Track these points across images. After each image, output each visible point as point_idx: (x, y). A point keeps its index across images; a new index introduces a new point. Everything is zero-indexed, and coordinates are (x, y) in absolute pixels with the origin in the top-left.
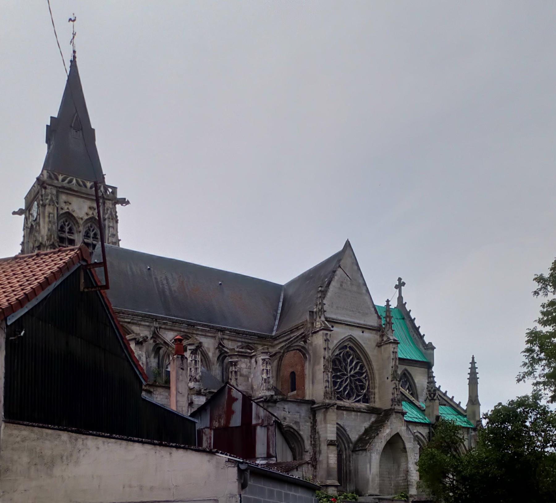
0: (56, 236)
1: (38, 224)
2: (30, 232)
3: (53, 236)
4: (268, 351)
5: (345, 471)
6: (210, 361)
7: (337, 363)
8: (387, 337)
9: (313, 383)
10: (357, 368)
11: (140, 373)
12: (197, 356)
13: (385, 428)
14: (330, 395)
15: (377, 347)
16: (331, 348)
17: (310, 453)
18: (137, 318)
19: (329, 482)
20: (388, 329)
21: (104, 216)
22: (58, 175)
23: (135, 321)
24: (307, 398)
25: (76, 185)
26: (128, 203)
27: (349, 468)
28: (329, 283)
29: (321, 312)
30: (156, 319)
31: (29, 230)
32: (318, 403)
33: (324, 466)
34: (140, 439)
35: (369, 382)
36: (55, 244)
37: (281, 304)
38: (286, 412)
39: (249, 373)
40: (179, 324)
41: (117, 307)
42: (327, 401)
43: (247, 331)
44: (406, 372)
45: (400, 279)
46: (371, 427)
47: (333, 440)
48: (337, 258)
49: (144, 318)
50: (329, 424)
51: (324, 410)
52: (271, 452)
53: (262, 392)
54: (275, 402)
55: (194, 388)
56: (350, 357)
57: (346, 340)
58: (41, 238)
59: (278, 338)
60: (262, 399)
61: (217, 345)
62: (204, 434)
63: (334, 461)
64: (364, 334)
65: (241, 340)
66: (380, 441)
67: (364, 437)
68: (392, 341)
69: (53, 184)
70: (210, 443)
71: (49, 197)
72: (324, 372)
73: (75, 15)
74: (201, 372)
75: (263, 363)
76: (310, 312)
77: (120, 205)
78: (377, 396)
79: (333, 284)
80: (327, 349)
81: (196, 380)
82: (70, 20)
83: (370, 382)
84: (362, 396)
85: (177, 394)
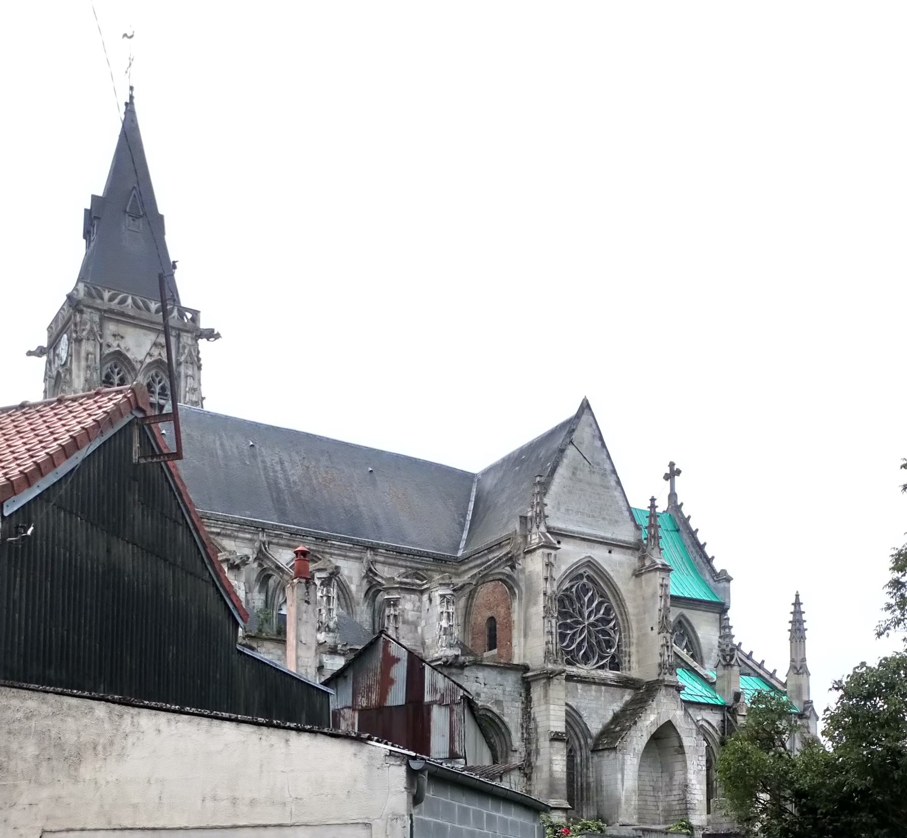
1: (69, 371)
2: (56, 383)
4: (450, 582)
5: (579, 784)
6: (353, 598)
7: (567, 602)
8: (651, 559)
9: (525, 636)
10: (600, 611)
12: (332, 589)
13: (649, 712)
15: (634, 577)
17: (520, 753)
18: (232, 526)
19: (552, 803)
23: (229, 532)
25: (132, 307)
26: (217, 336)
28: (554, 470)
29: (540, 519)
30: (262, 528)
31: (53, 381)
33: (545, 775)
34: (234, 716)
35: (620, 635)
37: (471, 506)
39: (418, 618)
40: (301, 537)
42: (550, 666)
44: (682, 620)
45: (672, 465)
46: (623, 710)
47: (559, 733)
48: (569, 427)
49: (242, 527)
51: (545, 681)
52: (457, 749)
53: (440, 651)
55: (325, 642)
56: (588, 593)
59: (466, 561)
60: (439, 662)
62: (341, 719)
65: (404, 563)
66: (640, 735)
68: (660, 566)
69: (95, 306)
71: (88, 327)
72: (544, 618)
75: (442, 602)
76: (521, 517)
81: (329, 630)
82: (125, 35)
83: (623, 634)
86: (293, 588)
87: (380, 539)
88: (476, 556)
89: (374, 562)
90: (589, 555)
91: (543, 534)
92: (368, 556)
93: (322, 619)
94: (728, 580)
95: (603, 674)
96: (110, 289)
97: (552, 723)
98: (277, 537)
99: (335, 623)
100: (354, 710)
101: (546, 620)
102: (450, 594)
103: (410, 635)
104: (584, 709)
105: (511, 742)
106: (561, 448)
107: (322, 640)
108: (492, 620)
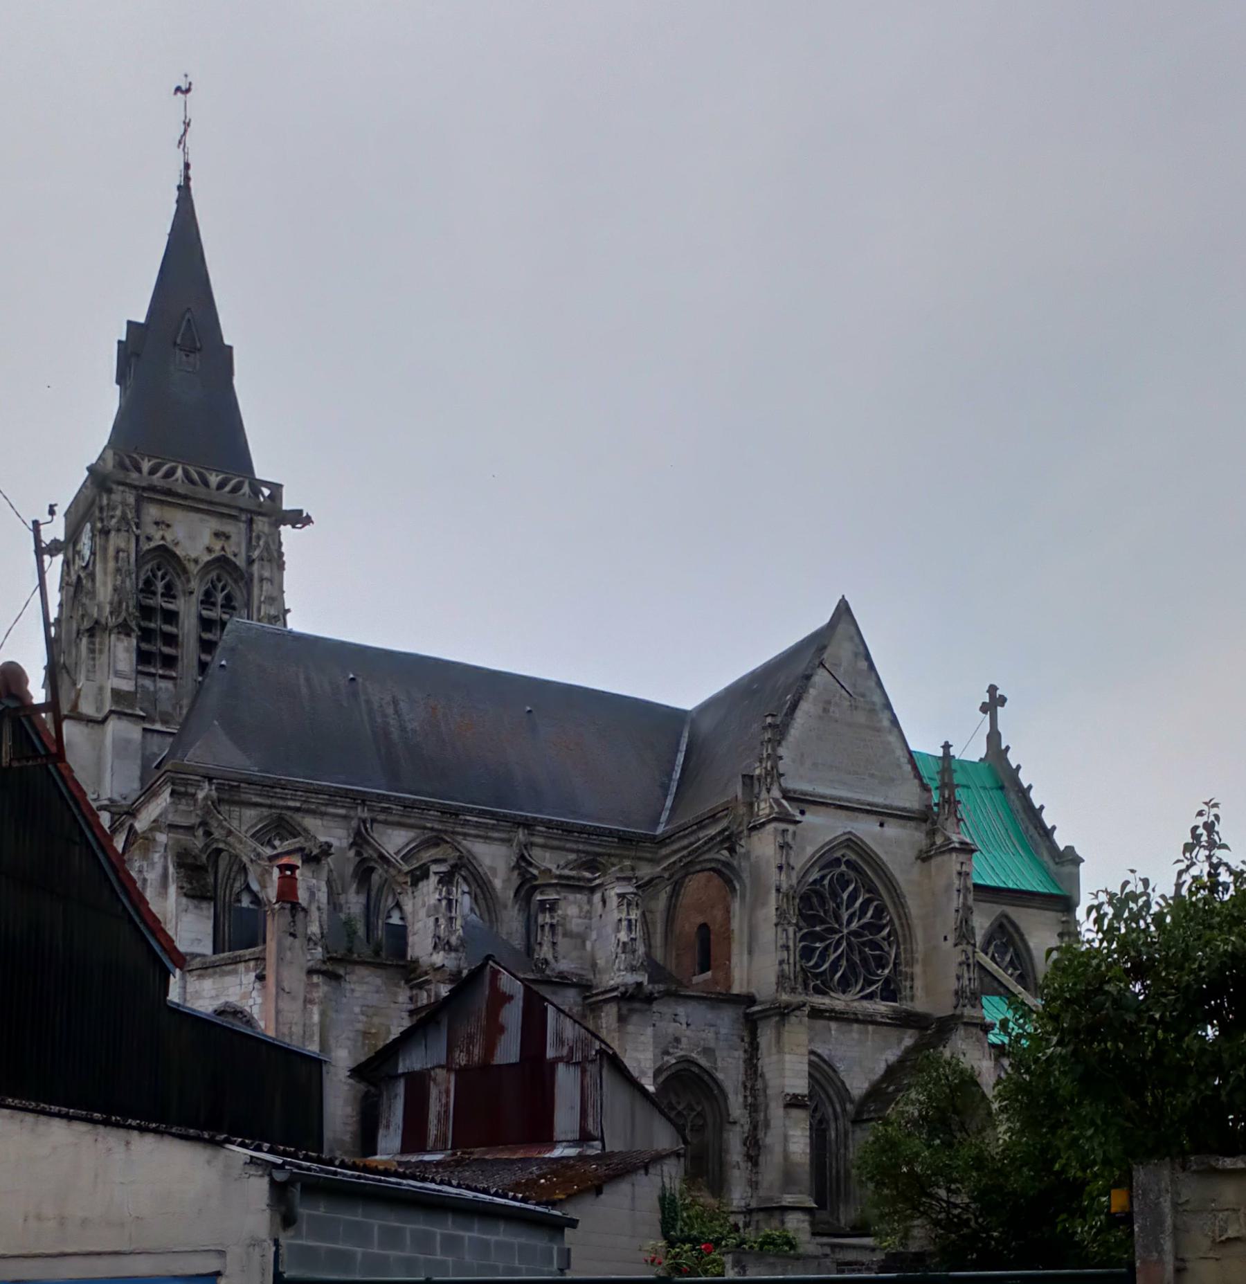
0: (132, 603)
1: (92, 576)
2: (75, 592)
3: (124, 604)
4: (632, 876)
5: (834, 1171)
6: (497, 897)
7: (815, 900)
8: (944, 835)
10: (866, 913)
11: (164, 949)
12: (454, 889)
14: (793, 983)
15: (919, 861)
16: (798, 866)
17: (742, 1126)
18: (317, 798)
19: (788, 1200)
20: (946, 816)
21: (251, 554)
22: (140, 460)
24: (736, 990)
25: (183, 481)
26: (308, 520)
27: (845, 1164)
28: (794, 706)
29: (772, 778)
30: (362, 799)
31: (72, 589)
32: (762, 1003)
33: (777, 1157)
34: (64, 1110)
35: (898, 948)
36: (129, 622)
37: (681, 758)
38: (681, 1024)
39: (586, 928)
40: (420, 811)
41: (268, 772)
42: (785, 997)
43: (590, 826)
44: (1005, 921)
45: (992, 689)
46: (901, 1061)
47: (798, 1095)
48: (817, 644)
49: (333, 798)
50: (790, 1053)
51: (777, 1018)
52: (591, 1126)
53: (618, 976)
54: (650, 999)
55: (443, 966)
56: (848, 886)
57: (839, 844)
58: (96, 609)
59: (668, 841)
60: (615, 994)
61: (515, 859)
62: (432, 1083)
63: (802, 1146)
64: (886, 828)
67: (884, 1086)
68: (957, 845)
69: (128, 481)
70: (447, 1104)
71: (118, 513)
72: (776, 925)
73: (190, 79)
74: (462, 927)
75: (620, 905)
76: (744, 776)
77: (289, 527)
78: (918, 983)
79: (804, 706)
80: (784, 869)
81: (449, 948)
82: (178, 89)
83: (902, 947)
84: (880, 983)
85: (277, 993)
86: (274, 917)
87: (540, 812)
88: (681, 834)
89: (528, 845)
90: (849, 829)
91: (776, 801)
92: (521, 836)
93: (439, 932)
94: (1077, 861)
95: (869, 1006)
96: (150, 457)
97: (787, 1082)
98: (384, 812)
99: (459, 938)
100: (449, 1070)
101: (779, 929)
102: (632, 893)
103: (575, 954)
104: (840, 1059)
105: (727, 1110)
106: (807, 673)
107: (439, 964)
108: (704, 927)
